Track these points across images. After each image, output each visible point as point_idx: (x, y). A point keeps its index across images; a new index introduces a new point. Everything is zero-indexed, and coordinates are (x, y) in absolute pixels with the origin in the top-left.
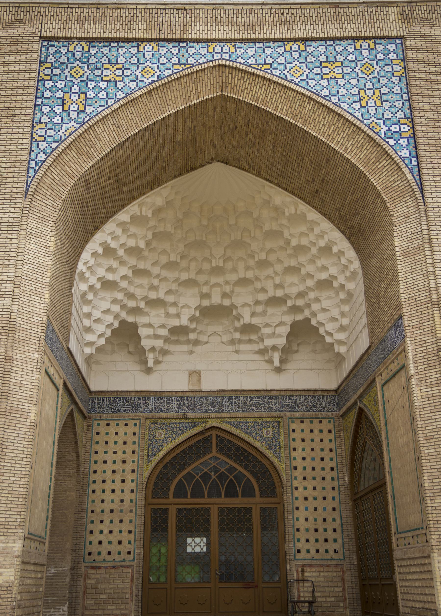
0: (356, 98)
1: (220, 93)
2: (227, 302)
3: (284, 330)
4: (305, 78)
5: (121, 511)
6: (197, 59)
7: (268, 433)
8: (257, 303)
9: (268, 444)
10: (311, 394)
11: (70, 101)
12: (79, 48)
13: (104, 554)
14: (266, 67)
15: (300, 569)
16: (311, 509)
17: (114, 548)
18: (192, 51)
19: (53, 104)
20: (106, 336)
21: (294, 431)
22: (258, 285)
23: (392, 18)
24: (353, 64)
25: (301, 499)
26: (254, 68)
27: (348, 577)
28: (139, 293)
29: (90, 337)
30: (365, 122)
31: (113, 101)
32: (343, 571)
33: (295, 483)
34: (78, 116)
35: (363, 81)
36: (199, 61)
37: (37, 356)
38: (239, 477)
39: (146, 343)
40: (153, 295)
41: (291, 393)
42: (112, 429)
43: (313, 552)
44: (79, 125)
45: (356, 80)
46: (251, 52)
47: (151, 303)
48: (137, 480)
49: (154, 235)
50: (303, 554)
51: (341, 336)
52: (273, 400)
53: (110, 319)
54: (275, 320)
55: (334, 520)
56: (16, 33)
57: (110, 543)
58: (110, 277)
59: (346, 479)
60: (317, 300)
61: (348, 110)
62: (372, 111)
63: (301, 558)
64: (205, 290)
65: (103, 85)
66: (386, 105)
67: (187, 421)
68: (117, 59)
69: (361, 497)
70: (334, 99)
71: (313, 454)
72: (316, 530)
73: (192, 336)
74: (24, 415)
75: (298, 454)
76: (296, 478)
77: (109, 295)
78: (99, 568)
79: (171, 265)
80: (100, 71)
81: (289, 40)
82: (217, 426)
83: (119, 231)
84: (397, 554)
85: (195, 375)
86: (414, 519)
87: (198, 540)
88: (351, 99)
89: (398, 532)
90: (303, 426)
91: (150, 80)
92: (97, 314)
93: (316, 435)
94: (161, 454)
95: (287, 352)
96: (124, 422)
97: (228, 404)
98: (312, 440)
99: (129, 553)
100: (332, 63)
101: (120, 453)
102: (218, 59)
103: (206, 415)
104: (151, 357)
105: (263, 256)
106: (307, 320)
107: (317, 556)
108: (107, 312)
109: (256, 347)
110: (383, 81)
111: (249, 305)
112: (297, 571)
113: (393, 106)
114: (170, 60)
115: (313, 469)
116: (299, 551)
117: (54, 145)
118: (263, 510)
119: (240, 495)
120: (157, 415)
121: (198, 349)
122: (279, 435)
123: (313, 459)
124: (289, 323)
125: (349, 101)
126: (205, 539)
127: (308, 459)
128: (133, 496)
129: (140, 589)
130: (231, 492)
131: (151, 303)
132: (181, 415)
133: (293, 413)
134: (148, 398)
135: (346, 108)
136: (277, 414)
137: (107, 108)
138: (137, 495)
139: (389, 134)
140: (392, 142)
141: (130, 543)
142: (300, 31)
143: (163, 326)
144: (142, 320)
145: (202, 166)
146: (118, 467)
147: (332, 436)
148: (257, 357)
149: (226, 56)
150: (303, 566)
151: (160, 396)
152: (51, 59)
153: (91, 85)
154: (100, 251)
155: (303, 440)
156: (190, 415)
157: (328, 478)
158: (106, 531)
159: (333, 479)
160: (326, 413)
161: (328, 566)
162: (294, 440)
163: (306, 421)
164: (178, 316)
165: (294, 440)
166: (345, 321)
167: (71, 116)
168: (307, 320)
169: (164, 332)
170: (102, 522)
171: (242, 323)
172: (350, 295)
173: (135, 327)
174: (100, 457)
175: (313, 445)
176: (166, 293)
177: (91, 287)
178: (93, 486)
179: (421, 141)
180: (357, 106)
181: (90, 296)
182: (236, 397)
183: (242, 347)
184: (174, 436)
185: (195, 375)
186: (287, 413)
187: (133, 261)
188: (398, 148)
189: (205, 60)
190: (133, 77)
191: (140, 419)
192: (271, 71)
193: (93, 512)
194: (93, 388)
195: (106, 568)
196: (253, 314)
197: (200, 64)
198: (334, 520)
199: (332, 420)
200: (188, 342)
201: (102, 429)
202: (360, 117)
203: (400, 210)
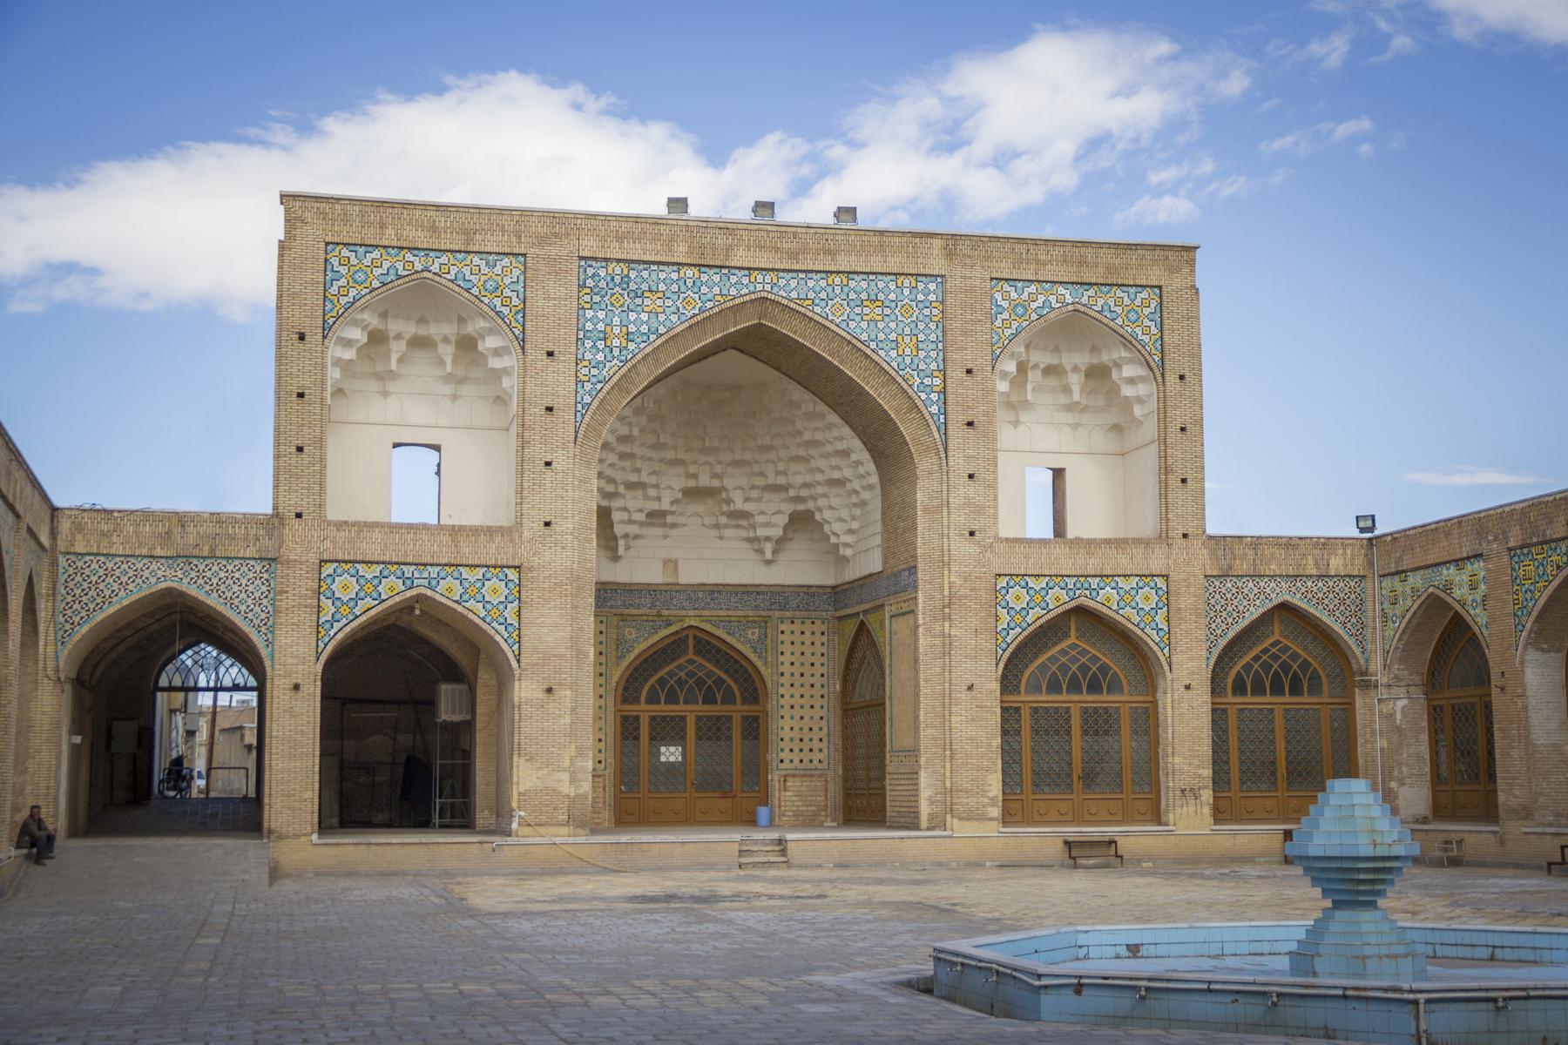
2: (716, 483)
3: (782, 520)
16: (797, 717)
18: (733, 279)
22: (756, 468)
23: (935, 252)
25: (787, 707)
27: (831, 786)
33: (781, 691)
35: (901, 325)
38: (719, 682)
39: (619, 529)
40: (634, 478)
43: (796, 761)
47: (631, 486)
50: (786, 764)
51: (848, 539)
54: (772, 508)
56: (554, 251)
60: (825, 496)
64: (692, 469)
65: (644, 317)
66: (922, 354)
70: (873, 345)
71: (803, 659)
75: (787, 659)
84: (889, 769)
86: (908, 742)
87: (672, 749)
90: (793, 627)
93: (808, 638)
94: (632, 656)
95: (780, 543)
104: (621, 542)
105: (767, 441)
109: (744, 534)
110: (921, 326)
117: (599, 386)
118: (745, 719)
120: (627, 611)
121: (675, 532)
130: (709, 699)
131: (631, 486)
132: (654, 612)
142: (844, 262)
143: (641, 510)
147: (825, 639)
148: (744, 545)
149: (768, 287)
152: (590, 283)
156: (665, 612)
163: (798, 622)
164: (659, 499)
166: (855, 525)
169: (641, 517)
175: (804, 649)
176: (672, 503)
179: (950, 397)
180: (893, 354)
183: (727, 532)
190: (673, 309)
200: (665, 525)
203: (924, 464)
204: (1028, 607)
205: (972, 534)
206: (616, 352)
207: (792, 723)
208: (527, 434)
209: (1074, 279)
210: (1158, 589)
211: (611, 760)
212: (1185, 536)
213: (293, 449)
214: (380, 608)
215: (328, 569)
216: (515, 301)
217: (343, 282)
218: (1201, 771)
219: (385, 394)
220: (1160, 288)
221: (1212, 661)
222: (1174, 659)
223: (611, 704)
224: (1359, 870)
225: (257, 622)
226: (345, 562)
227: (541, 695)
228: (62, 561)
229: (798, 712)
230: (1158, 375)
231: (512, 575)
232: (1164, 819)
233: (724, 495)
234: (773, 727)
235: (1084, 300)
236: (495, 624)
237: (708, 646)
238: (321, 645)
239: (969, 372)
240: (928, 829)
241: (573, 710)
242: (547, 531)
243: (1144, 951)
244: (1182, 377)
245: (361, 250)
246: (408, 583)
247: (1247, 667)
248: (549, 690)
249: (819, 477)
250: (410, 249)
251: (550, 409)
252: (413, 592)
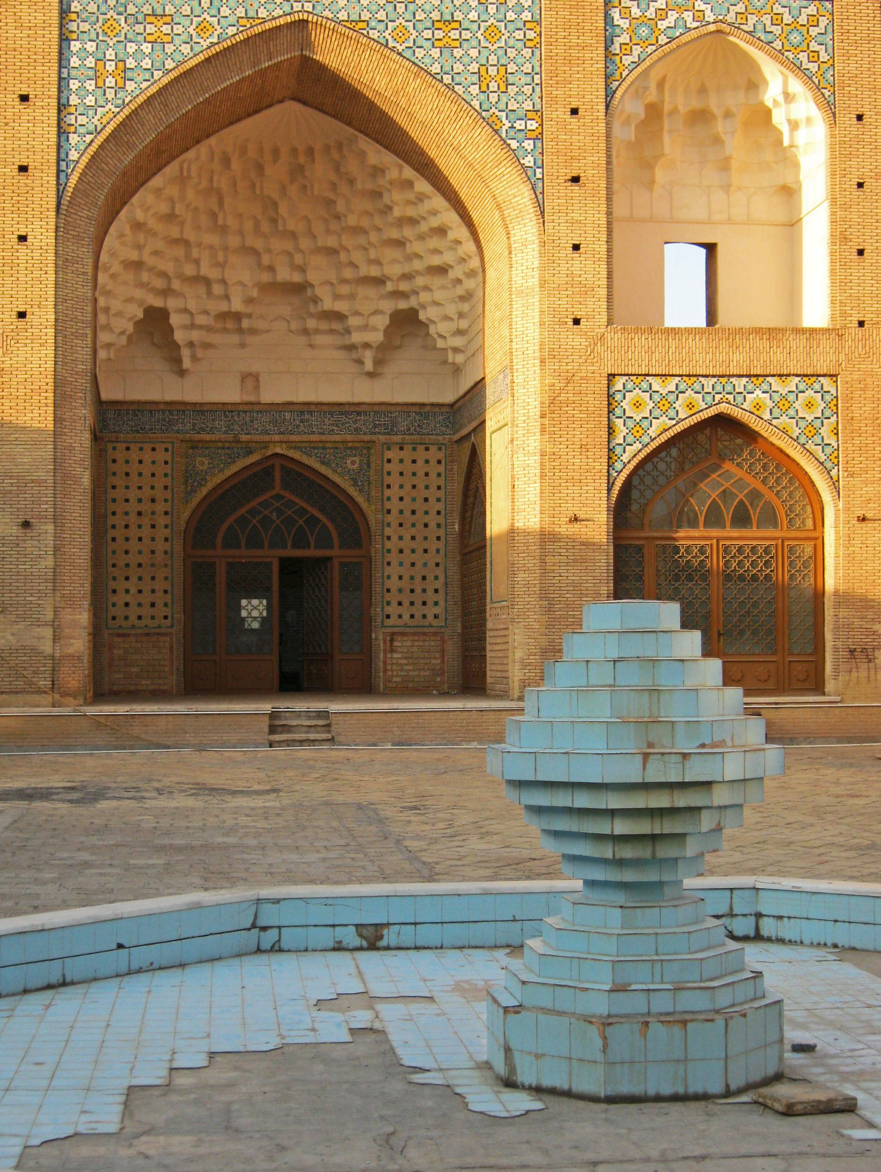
0: (475, 78)
1: (300, 53)
3: (382, 322)
4: (411, 45)
5: (153, 565)
6: (271, 11)
7: (353, 463)
8: (344, 281)
9: (353, 479)
10: (417, 409)
11: (105, 74)
13: (133, 618)
14: (361, 25)
15: (388, 638)
16: (407, 564)
17: (146, 611)
19: (82, 77)
20: (128, 333)
21: (389, 461)
24: (475, 27)
25: (395, 551)
26: (345, 26)
30: (484, 114)
31: (160, 73)
32: (443, 641)
34: (116, 95)
35: (485, 53)
36: (273, 14)
37: (84, 412)
38: (313, 521)
39: (179, 336)
41: (389, 408)
43: (406, 617)
44: (118, 110)
45: (477, 50)
48: (172, 525)
52: (362, 417)
55: (436, 578)
57: (140, 605)
59: (456, 527)
60: (427, 288)
61: (464, 96)
62: (493, 98)
63: (390, 624)
66: (512, 90)
67: (239, 445)
68: (164, 8)
69: (471, 552)
71: (414, 493)
72: (412, 591)
76: (389, 525)
78: (128, 635)
80: (142, 27)
82: (282, 452)
84: (489, 625)
87: (255, 602)
88: (469, 79)
89: (492, 603)
90: (402, 454)
91: (208, 41)
94: (205, 491)
95: (385, 352)
96: (151, 446)
97: (298, 422)
98: (414, 474)
99: (166, 617)
100: (447, 23)
102: (298, 12)
103: (266, 438)
104: (185, 353)
107: (411, 622)
111: (332, 284)
112: (385, 641)
113: (520, 92)
115: (413, 512)
116: (388, 616)
117: (89, 138)
119: (312, 546)
120: (198, 437)
122: (369, 467)
123: (414, 499)
124: (389, 312)
125: (466, 82)
126: (265, 602)
127: (407, 499)
128: (167, 547)
129: (182, 661)
132: (230, 437)
133: (388, 437)
134: (184, 411)
135: (461, 92)
136: (367, 438)
137: (152, 84)
138: (172, 544)
139: (512, 133)
141: (166, 605)
143: (206, 312)
144: (172, 304)
145: (270, 106)
146: (145, 507)
147: (441, 468)
148: (341, 354)
150: (393, 634)
151: (200, 409)
155: (401, 474)
156: (244, 438)
157: (433, 525)
158: (133, 591)
159: (439, 526)
160: (435, 437)
161: (424, 634)
162: (389, 473)
163: (408, 448)
165: (389, 473)
167: (108, 95)
170: (127, 578)
171: (320, 309)
178: (111, 533)
182: (311, 413)
183: (320, 339)
184: (222, 466)
185: (251, 379)
186: (381, 437)
188: (520, 153)
189: (281, 13)
190: (184, 37)
191: (173, 443)
192: (368, 33)
193: (114, 565)
195: (136, 635)
197: (274, 18)
198: (436, 578)
199: (443, 447)
200: (240, 331)
201: (120, 455)
202: (478, 108)
204: (651, 418)
205: (577, 322)
206: (110, 94)
207: (401, 571)
210: (823, 392)
211: (179, 616)
212: (861, 324)
223: (178, 548)
224: (612, 813)
227: (15, 530)
229: (407, 557)
233: (309, 292)
234: (377, 575)
235: (731, 17)
237: (299, 478)
239: (574, 111)
241: (56, 549)
242: (21, 323)
243: (390, 937)
248: (26, 525)
249: (418, 265)
251: (23, 169)
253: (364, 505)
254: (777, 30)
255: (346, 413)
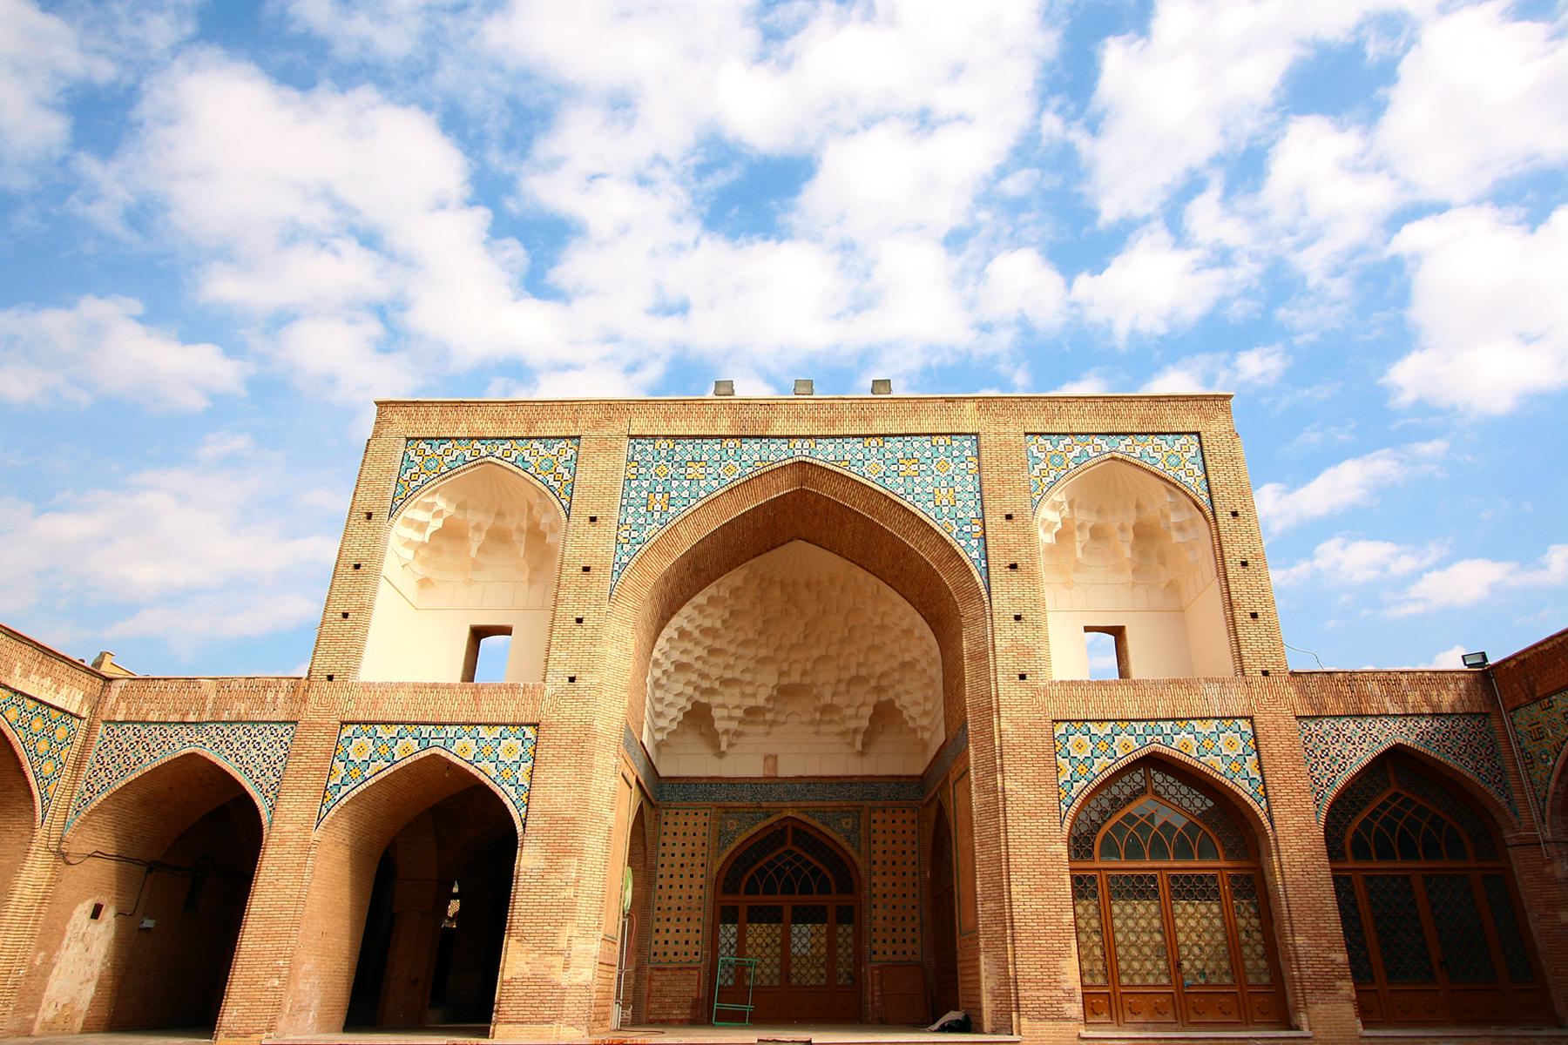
3: (868, 711)
12: (665, 445)
13: (670, 955)
28: (715, 672)
29: (662, 723)
38: (816, 871)
39: (720, 725)
40: (728, 674)
42: (681, 819)
43: (889, 953)
46: (831, 448)
47: (725, 682)
49: (731, 613)
51: (925, 721)
53: (682, 702)
54: (859, 700)
58: (685, 659)
64: (785, 667)
70: (910, 498)
73: (769, 716)
74: (603, 819)
77: (682, 677)
79: (745, 643)
81: (868, 436)
83: (695, 614)
84: (960, 957)
85: (771, 759)
92: (669, 698)
94: (733, 847)
101: (689, 845)
104: (724, 740)
106: (891, 702)
107: (895, 958)
108: (680, 694)
109: (836, 728)
114: (755, 455)
119: (834, 888)
121: (775, 729)
130: (806, 890)
131: (725, 682)
140: (963, 543)
143: (738, 707)
148: (838, 739)
151: (732, 782)
153: (675, 484)
154: (676, 635)
156: (765, 804)
158: (672, 930)
164: (754, 695)
168: (891, 702)
172: (933, 680)
173: (708, 707)
174: (667, 850)
177: (664, 672)
178: (660, 882)
180: (930, 505)
181: (664, 681)
183: (823, 728)
187: (708, 642)
194: (662, 774)
196: (835, 694)
200: (764, 722)
201: (671, 820)
204: (1093, 756)
208: (561, 593)
209: (1109, 430)
213: (339, 616)
214: (391, 770)
215: (348, 731)
216: (567, 476)
217: (416, 470)
218: (1333, 956)
219: (470, 582)
220: (1198, 434)
221: (1323, 815)
222: (1275, 812)
225: (266, 787)
226: (366, 723)
228: (101, 729)
230: (1211, 517)
231: (530, 732)
232: (1295, 1021)
236: (505, 786)
238: (324, 810)
239: (1009, 517)
240: (994, 1032)
244: (1235, 514)
245: (437, 443)
246: (424, 743)
247: (1365, 824)
250: (478, 439)
251: (586, 569)
252: (427, 753)
253: (855, 857)
254: (1158, 456)
255: (842, 784)
